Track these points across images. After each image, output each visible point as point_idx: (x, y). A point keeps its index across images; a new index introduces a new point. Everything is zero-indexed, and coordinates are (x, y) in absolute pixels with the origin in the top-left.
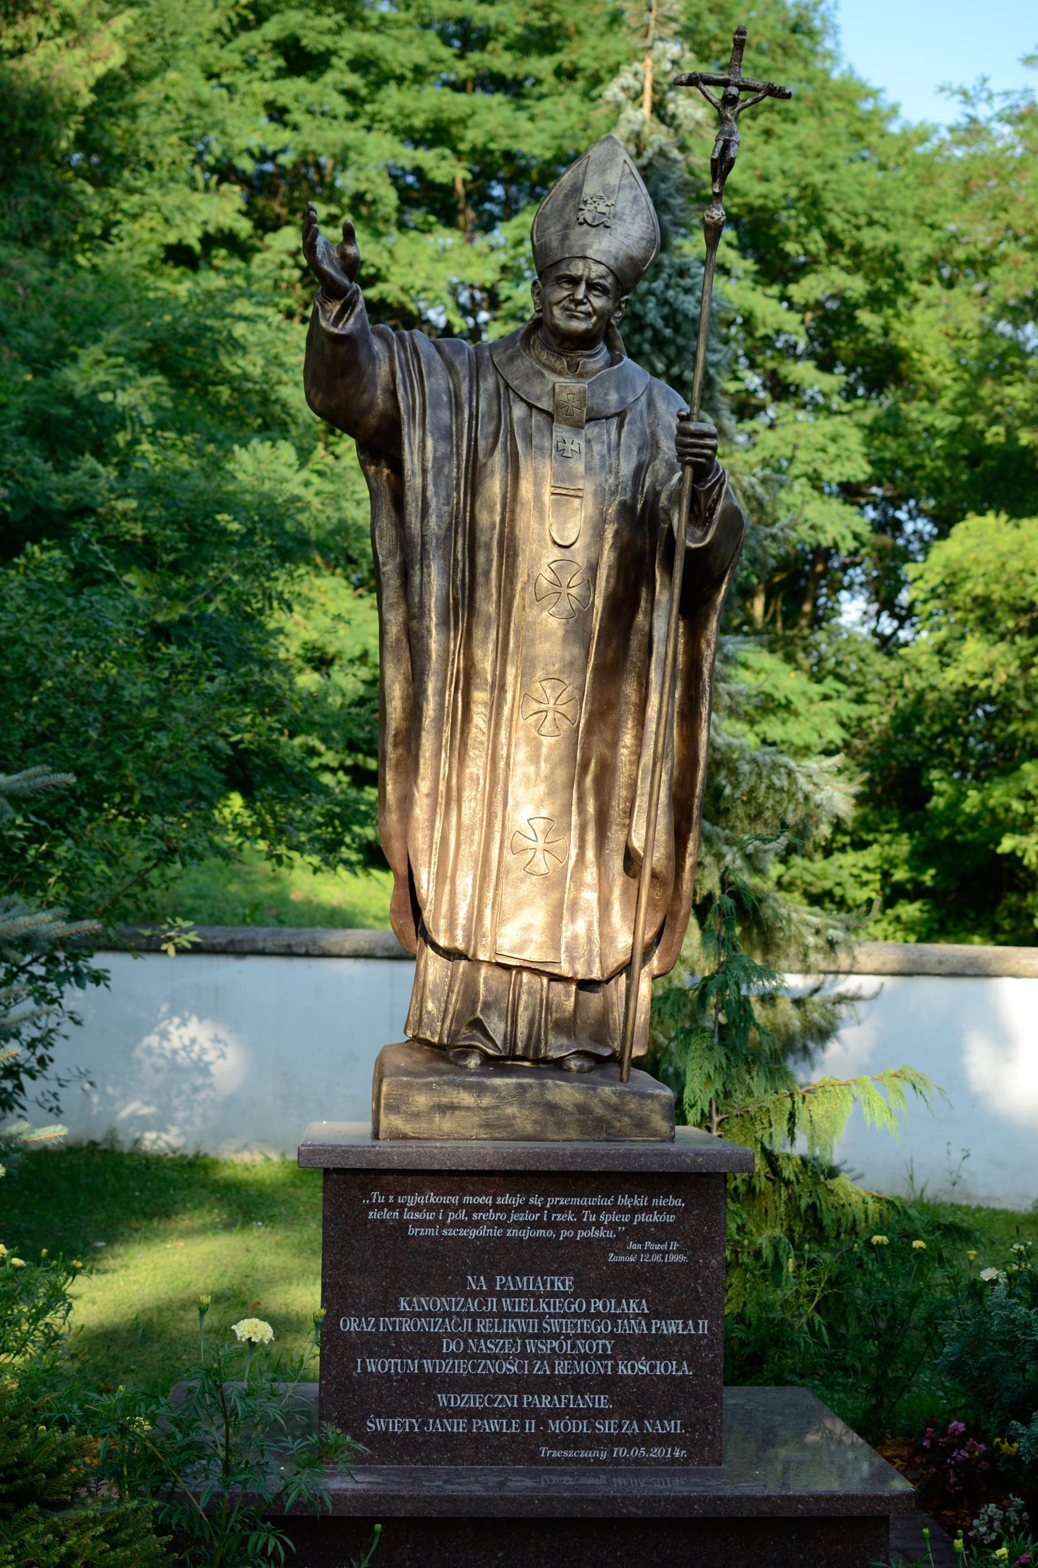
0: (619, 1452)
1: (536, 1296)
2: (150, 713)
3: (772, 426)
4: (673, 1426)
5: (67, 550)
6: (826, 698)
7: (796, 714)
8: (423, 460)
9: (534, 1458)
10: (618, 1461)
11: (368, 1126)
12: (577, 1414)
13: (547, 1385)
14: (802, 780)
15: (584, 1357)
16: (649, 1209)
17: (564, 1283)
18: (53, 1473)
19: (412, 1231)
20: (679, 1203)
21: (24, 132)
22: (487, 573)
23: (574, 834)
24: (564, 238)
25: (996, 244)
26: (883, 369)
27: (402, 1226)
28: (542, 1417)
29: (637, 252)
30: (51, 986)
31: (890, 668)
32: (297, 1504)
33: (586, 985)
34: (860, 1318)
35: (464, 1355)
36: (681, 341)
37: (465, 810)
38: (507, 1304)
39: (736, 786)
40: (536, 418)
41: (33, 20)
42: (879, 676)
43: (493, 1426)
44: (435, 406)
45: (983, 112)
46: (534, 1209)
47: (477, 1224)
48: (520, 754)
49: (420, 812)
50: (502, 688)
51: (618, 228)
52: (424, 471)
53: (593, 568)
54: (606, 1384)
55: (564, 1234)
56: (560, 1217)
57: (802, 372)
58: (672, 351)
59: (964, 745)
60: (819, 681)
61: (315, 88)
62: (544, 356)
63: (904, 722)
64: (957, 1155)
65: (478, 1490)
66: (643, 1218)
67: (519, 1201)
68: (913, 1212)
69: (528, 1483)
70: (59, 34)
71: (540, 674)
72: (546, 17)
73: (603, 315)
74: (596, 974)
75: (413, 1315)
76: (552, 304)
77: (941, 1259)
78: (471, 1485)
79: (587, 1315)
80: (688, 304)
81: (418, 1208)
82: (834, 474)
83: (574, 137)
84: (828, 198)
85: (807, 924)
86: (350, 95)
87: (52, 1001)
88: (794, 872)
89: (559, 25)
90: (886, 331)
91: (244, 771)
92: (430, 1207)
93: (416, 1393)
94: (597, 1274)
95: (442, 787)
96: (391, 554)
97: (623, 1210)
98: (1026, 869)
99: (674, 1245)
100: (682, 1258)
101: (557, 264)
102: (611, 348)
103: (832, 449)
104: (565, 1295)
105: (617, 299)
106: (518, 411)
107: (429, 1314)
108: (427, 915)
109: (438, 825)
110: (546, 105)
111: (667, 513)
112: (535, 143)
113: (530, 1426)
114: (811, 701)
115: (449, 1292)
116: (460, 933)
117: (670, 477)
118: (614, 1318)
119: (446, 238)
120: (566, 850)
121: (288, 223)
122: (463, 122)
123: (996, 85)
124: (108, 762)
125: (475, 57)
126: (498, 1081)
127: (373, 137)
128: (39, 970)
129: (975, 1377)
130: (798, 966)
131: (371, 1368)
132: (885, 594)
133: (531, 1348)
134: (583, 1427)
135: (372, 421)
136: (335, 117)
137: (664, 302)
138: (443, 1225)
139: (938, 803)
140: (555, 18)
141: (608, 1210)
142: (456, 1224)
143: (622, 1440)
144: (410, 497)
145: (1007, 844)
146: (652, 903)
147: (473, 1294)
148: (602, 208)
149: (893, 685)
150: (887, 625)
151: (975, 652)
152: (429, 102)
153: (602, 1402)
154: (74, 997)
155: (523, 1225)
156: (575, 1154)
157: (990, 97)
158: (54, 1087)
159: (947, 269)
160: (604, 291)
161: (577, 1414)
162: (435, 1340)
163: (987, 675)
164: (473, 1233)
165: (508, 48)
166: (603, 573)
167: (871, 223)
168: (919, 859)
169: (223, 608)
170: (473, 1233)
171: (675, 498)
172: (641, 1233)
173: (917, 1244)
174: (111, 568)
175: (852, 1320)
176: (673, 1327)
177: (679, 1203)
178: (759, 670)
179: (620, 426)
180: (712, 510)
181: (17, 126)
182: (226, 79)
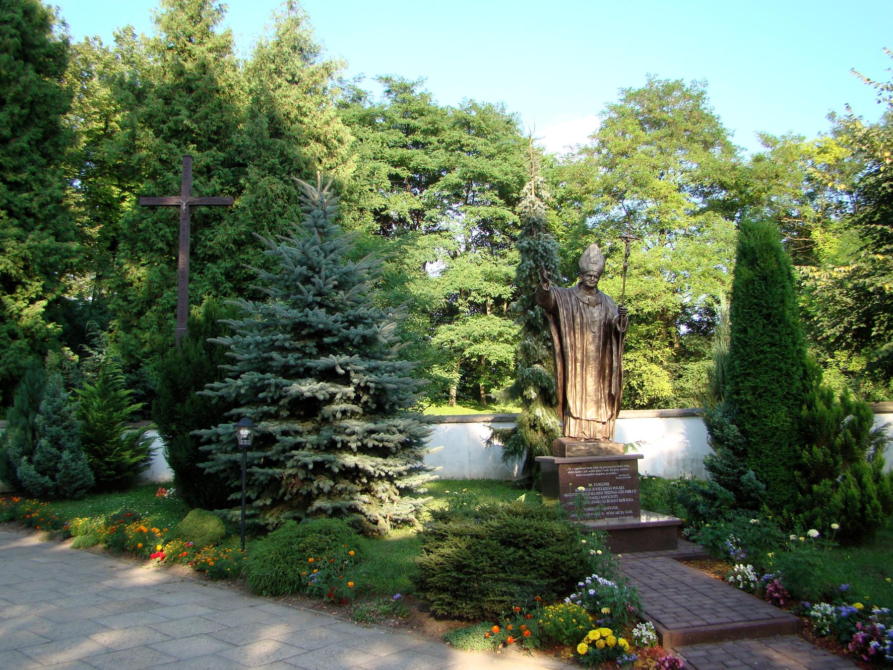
4: (631, 512)
12: (611, 510)
17: (607, 484)
33: (604, 423)
54: (617, 504)
80: (550, 246)
122: (410, 159)
137: (543, 246)
153: (616, 508)
161: (611, 510)
176: (629, 491)
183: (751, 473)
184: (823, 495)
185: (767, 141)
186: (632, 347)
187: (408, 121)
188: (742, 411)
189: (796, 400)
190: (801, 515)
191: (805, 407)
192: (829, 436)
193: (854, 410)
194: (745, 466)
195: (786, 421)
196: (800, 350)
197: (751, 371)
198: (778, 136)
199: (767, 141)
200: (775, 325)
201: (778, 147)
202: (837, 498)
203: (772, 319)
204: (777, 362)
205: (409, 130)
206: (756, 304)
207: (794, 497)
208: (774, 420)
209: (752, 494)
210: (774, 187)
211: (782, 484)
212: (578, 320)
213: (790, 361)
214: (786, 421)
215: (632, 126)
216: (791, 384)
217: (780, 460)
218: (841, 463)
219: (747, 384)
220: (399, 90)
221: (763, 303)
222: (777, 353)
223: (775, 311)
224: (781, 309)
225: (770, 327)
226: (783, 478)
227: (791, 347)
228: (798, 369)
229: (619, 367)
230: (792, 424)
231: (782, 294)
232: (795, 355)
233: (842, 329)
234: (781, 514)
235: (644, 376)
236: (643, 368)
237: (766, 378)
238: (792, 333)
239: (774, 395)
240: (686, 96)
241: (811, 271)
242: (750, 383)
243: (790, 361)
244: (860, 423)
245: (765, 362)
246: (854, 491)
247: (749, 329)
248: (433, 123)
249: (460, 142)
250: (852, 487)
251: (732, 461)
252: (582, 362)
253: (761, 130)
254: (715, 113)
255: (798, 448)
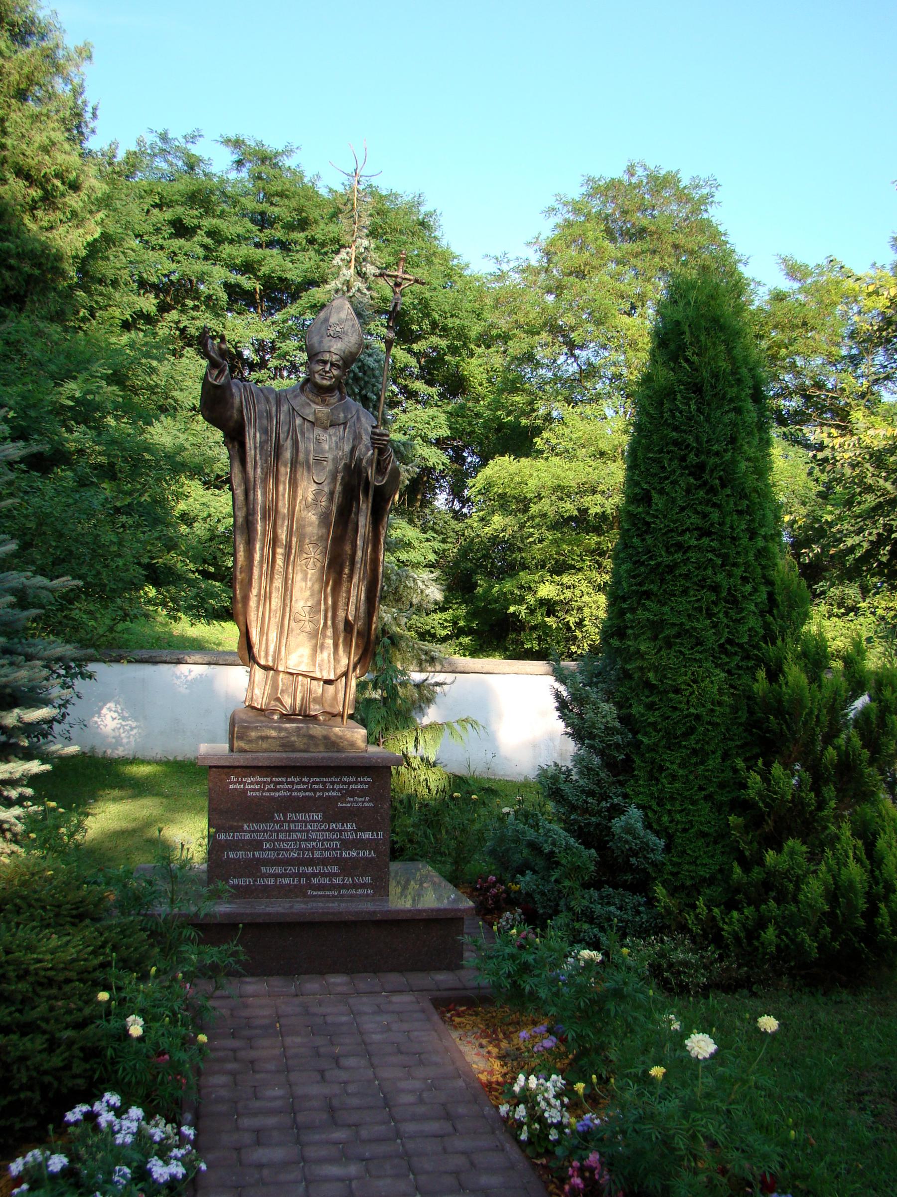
0: (343, 892)
1: (306, 822)
2: (114, 548)
3: (404, 411)
4: (367, 880)
5: (74, 471)
6: (428, 540)
7: (414, 548)
8: (255, 443)
9: (305, 895)
10: (343, 896)
11: (227, 746)
12: (324, 875)
13: (311, 862)
14: (420, 584)
15: (328, 849)
16: (356, 783)
17: (318, 816)
18: (96, 905)
19: (249, 794)
20: (369, 780)
21: (53, 268)
22: (284, 495)
23: (322, 613)
24: (321, 342)
25: (510, 330)
26: (456, 385)
27: (245, 791)
28: (308, 877)
29: (354, 350)
30: (68, 679)
31: (459, 526)
32: (206, 915)
33: (328, 682)
34: (447, 832)
35: (274, 850)
36: (366, 379)
37: (273, 603)
38: (292, 826)
39: (389, 586)
40: (307, 424)
41: (58, 213)
42: (453, 530)
43: (286, 881)
44: (261, 418)
45: (505, 267)
46: (304, 783)
47: (279, 790)
48: (298, 577)
49: (253, 603)
50: (290, 547)
51: (342, 332)
52: (255, 448)
53: (332, 493)
55: (318, 794)
56: (316, 787)
57: (419, 386)
58: (362, 383)
59: (492, 563)
60: (425, 533)
61: (189, 244)
62: (310, 396)
63: (464, 553)
64: (490, 756)
65: (281, 910)
66: (353, 786)
67: (297, 779)
68: (471, 782)
69: (303, 906)
70: (70, 220)
71: (307, 541)
72: (300, 214)
73: (338, 378)
74: (332, 677)
75: (250, 831)
76: (315, 372)
77: (484, 803)
78: (277, 907)
79: (328, 830)
81: (252, 783)
82: (433, 435)
83: (312, 272)
84: (433, 304)
85: (422, 650)
86: (205, 247)
87: (69, 687)
88: (412, 622)
89: (307, 218)
90: (457, 367)
91: (158, 576)
92: (257, 783)
93: (252, 867)
94: (334, 813)
95: (263, 592)
96: (240, 485)
97: (344, 783)
98: (520, 621)
99: (368, 799)
100: (371, 804)
101: (317, 354)
102: (341, 392)
103: (432, 423)
104: (318, 821)
105: (344, 371)
106: (298, 421)
107: (258, 831)
108: (256, 650)
109: (261, 609)
110: (299, 256)
111: (366, 468)
112: (294, 274)
113: (303, 881)
114: (421, 542)
115: (266, 821)
116: (270, 658)
117: (367, 453)
118: (341, 831)
119: (252, 316)
120: (319, 621)
121: (174, 308)
122: (259, 262)
123: (511, 256)
124: (94, 572)
125: (267, 231)
126: (288, 725)
127: (217, 267)
128: (63, 672)
129: (501, 857)
130: (417, 669)
131: (231, 856)
132: (457, 492)
133: (303, 846)
134: (327, 881)
135: (231, 424)
136: (199, 258)
138: (264, 791)
139: (479, 590)
140: (304, 214)
141: (338, 783)
142: (269, 790)
143: (344, 886)
144: (249, 460)
145: (512, 609)
146: (357, 645)
147: (277, 822)
148: (338, 329)
149: (459, 534)
150: (457, 506)
151: (498, 520)
152: (245, 251)
153: (335, 869)
154: (78, 683)
155: (299, 790)
156: (323, 758)
157: (508, 261)
158: (68, 728)
159: (486, 340)
160: (338, 367)
161: (324, 875)
162: (260, 843)
163: (503, 531)
164: (277, 794)
165: (283, 228)
166: (337, 495)
167: (452, 316)
168: (472, 615)
169: (149, 499)
170: (277, 794)
171: (370, 462)
172: (352, 793)
173: (474, 797)
174: (95, 480)
175: (443, 832)
176: (367, 835)
177: (369, 780)
178: (400, 529)
179: (345, 429)
180: (386, 468)
181: (49, 265)
182: (145, 238)
183: (634, 813)
184: (786, 874)
185: (794, 271)
186: (574, 567)
187: (265, 206)
188: (627, 675)
189: (747, 657)
190: (735, 914)
191: (761, 674)
192: (813, 742)
193: (872, 683)
194: (625, 796)
195: (720, 704)
196: (765, 549)
197: (654, 588)
198: (812, 265)
199: (794, 271)
200: (712, 490)
201: (809, 281)
202: (814, 889)
203: (706, 476)
204: (709, 572)
205: (263, 221)
206: (675, 443)
207: (724, 872)
208: (693, 699)
209: (633, 860)
210: (800, 340)
211: (701, 842)
212: (287, 455)
213: (739, 572)
214: (720, 704)
215: (595, 231)
216: (738, 621)
217: (701, 789)
218: (833, 804)
219: (642, 615)
220: (260, 160)
221: (690, 439)
222: (713, 550)
223: (713, 460)
224: (728, 456)
225: (701, 493)
226: (705, 829)
227: (745, 541)
228: (755, 590)
229: (375, 561)
230: (735, 709)
231: (734, 424)
232: (751, 557)
233: (873, 538)
234: (694, 907)
235: (586, 611)
236: (586, 598)
237: (683, 604)
238: (749, 511)
239: (699, 643)
240: (683, 197)
241: (829, 435)
242: (648, 615)
243: (739, 572)
244: (882, 718)
245: (683, 570)
246: (855, 872)
247: (654, 495)
248: (300, 210)
249: (339, 240)
250: (851, 862)
251: (599, 783)
252: (289, 547)
253: (785, 253)
254: (721, 229)
255: (740, 763)
